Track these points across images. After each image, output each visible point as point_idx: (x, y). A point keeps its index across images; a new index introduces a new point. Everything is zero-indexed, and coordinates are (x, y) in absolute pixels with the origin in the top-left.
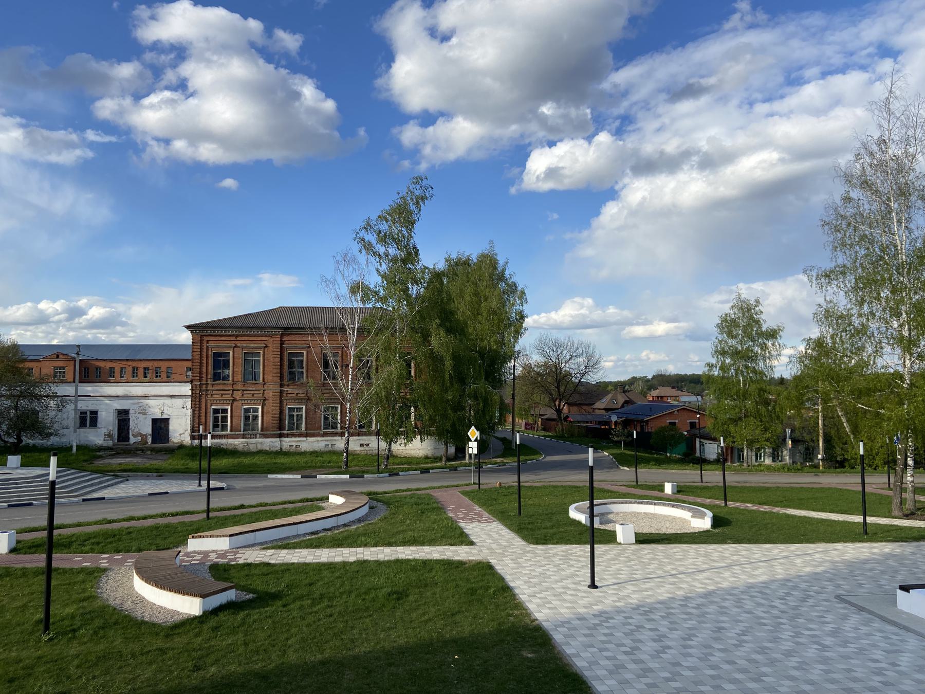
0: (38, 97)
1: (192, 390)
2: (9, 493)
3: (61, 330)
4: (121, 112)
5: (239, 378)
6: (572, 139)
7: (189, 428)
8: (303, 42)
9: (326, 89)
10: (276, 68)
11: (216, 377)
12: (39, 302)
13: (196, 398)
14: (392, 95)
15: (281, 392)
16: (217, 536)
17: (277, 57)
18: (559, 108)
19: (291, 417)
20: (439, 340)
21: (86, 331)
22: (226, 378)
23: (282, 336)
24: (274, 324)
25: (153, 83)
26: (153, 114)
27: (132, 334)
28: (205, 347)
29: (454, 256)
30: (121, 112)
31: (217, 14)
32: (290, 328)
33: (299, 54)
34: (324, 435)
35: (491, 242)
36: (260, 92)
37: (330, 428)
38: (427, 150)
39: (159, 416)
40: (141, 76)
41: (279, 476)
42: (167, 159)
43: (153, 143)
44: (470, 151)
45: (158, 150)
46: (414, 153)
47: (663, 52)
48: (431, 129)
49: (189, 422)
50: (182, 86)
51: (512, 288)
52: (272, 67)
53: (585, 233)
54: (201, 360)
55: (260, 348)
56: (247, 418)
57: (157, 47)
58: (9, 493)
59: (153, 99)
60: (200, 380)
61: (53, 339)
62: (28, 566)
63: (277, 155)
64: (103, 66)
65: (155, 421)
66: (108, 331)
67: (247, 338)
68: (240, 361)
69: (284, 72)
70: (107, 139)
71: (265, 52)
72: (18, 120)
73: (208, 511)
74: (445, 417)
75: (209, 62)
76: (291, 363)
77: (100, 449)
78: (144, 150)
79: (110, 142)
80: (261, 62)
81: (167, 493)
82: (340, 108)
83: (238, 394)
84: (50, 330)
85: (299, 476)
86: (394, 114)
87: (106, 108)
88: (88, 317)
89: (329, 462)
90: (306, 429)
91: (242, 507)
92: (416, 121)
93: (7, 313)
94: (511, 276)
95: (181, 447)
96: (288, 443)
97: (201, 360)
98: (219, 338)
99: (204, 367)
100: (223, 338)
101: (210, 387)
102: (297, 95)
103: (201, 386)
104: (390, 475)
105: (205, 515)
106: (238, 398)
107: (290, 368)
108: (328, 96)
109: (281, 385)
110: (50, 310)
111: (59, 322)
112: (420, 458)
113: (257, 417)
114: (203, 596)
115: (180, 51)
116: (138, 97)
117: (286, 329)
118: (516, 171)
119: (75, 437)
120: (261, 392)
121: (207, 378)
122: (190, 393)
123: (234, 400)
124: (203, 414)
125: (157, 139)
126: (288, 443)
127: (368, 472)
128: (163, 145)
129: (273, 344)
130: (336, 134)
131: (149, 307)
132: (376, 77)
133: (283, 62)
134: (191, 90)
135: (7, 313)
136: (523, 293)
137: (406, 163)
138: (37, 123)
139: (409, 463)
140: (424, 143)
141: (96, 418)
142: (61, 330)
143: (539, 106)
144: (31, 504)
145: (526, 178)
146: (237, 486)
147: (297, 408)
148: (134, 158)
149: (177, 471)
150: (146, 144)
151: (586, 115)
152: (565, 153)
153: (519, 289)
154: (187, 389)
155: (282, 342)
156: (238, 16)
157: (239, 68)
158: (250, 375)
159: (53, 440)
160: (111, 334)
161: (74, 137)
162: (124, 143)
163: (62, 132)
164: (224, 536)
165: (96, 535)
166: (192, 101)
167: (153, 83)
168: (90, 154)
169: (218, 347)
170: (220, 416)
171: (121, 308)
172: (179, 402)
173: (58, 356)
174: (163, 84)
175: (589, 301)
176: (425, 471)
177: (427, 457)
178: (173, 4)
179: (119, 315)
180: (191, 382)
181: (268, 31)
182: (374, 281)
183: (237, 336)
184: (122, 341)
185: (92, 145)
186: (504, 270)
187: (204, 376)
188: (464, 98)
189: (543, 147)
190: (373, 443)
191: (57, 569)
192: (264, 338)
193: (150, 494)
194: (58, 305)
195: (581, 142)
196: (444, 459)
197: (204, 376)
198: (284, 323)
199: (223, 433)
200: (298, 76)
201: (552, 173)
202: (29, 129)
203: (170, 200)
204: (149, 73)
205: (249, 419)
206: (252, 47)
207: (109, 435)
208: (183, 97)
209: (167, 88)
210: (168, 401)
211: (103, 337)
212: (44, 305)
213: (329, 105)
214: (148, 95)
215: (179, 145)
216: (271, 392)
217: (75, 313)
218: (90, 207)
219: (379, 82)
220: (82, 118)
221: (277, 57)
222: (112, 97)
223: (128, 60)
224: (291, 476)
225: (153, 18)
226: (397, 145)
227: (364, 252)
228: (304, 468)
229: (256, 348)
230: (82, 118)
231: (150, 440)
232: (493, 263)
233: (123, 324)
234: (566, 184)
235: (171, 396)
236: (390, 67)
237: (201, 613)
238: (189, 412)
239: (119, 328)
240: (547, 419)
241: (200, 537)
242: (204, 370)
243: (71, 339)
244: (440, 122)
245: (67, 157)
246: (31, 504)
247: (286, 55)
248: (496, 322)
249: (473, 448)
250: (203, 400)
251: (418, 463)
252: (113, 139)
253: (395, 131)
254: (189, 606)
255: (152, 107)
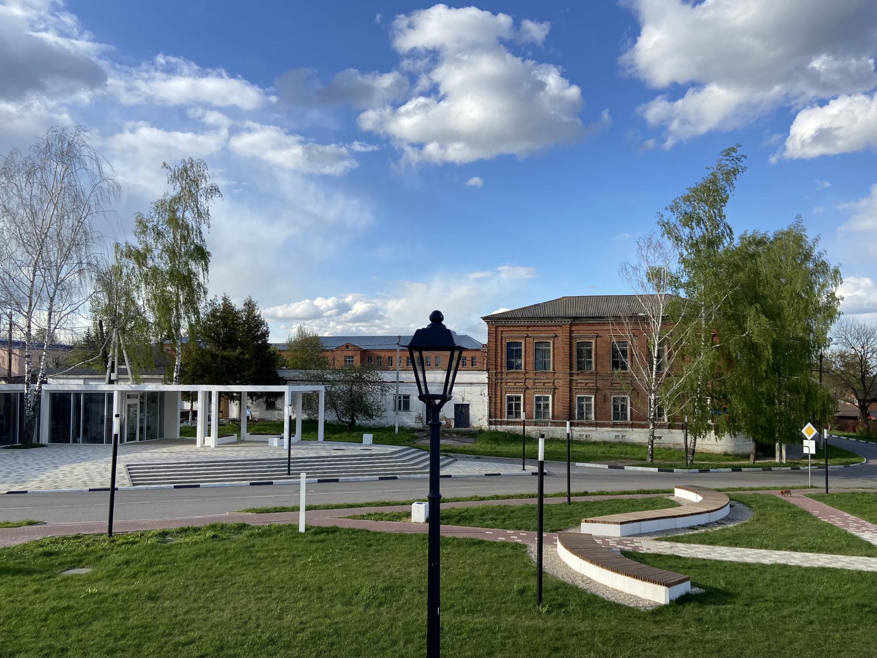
0: (314, 116)
1: (489, 378)
2: (376, 467)
3: (332, 324)
4: (382, 122)
5: (530, 367)
6: (850, 96)
7: (486, 413)
8: (550, 31)
9: (570, 76)
10: (523, 61)
11: (510, 366)
12: (314, 300)
13: (493, 386)
14: (637, 71)
15: (571, 381)
16: (609, 523)
17: (523, 49)
18: (836, 59)
19: (580, 407)
20: (756, 325)
21: (350, 324)
22: (519, 367)
23: (571, 325)
24: (562, 314)
25: (409, 90)
26: (408, 122)
27: (387, 327)
28: (499, 338)
29: (749, 233)
30: (382, 122)
31: (470, 14)
32: (579, 318)
33: (544, 43)
34: (614, 425)
35: (798, 216)
36: (508, 86)
37: (618, 417)
38: (675, 125)
39: (461, 402)
40: (398, 84)
41: (587, 465)
42: (420, 163)
43: (409, 149)
44: (724, 120)
45: (413, 155)
46: (661, 130)
47: (638, 12)
48: (680, 102)
49: (486, 408)
50: (434, 92)
51: (822, 267)
52: (519, 60)
53: (864, 202)
54: (496, 350)
55: (550, 338)
56: (538, 406)
57: (414, 54)
58: (376, 467)
59: (410, 106)
60: (496, 369)
61: (325, 331)
62: (457, 536)
63: (518, 148)
64: (367, 80)
65: (457, 406)
66: (369, 324)
67: (538, 328)
68: (531, 351)
69: (530, 63)
70: (370, 148)
71: (512, 46)
72: (298, 138)
73: (569, 495)
74: (759, 411)
75: (459, 62)
76: (579, 352)
77: (413, 430)
78: (401, 157)
79: (373, 151)
80: (509, 56)
81: (499, 475)
82: (584, 94)
83: (530, 383)
84: (322, 323)
85: (607, 466)
86: (641, 91)
87: (369, 119)
88: (353, 312)
89: (626, 453)
90: (596, 419)
91: (586, 494)
92: (664, 96)
93: (290, 309)
94: (820, 254)
95: (481, 431)
96: (579, 432)
97: (496, 350)
98: (511, 328)
99: (499, 356)
100: (516, 329)
101: (504, 376)
102: (542, 85)
103: (496, 374)
104: (701, 471)
105: (566, 499)
106: (530, 386)
107: (579, 357)
108: (571, 83)
109: (571, 375)
110: (323, 307)
111: (331, 316)
112: (719, 455)
113: (548, 405)
114: (668, 585)
115: (433, 56)
116: (396, 105)
117: (575, 318)
118: (777, 137)
119: (393, 418)
120: (551, 381)
121: (501, 366)
122: (487, 381)
123: (527, 388)
124: (499, 401)
125: (412, 145)
126: (579, 432)
127: (676, 467)
128: (417, 149)
129: (563, 334)
130: (579, 121)
131: (402, 301)
132: (620, 54)
133: (530, 54)
134: (442, 93)
135: (290, 309)
136: (836, 272)
137: (651, 143)
138: (314, 139)
139: (710, 459)
140: (671, 119)
141: (408, 402)
142: (332, 324)
143: (811, 61)
144: (396, 478)
145: (789, 143)
146: (555, 472)
147: (586, 398)
148: (393, 165)
149: (491, 454)
150: (402, 151)
151: (868, 66)
152: (840, 112)
153: (832, 268)
154: (483, 377)
155: (571, 332)
156: (489, 13)
157: (488, 65)
158: (541, 365)
159: (375, 422)
160: (372, 326)
161: (344, 150)
162: (385, 148)
163: (333, 146)
164: (615, 523)
165: (493, 510)
166: (444, 105)
167: (409, 90)
168: (356, 164)
169: (511, 337)
170: (514, 403)
171: (379, 303)
172: (477, 389)
173: (347, 347)
174: (418, 89)
175: (867, 281)
176: (737, 469)
177: (726, 454)
178: (429, 10)
179: (377, 310)
180: (488, 370)
181: (517, 25)
182: (675, 267)
183: (529, 327)
184: (379, 333)
185: (357, 156)
186: (811, 249)
187: (499, 364)
188: (721, 62)
189: (812, 107)
190: (676, 438)
191: (447, 542)
192: (554, 328)
193: (486, 475)
194: (330, 302)
195: (863, 98)
196: (752, 457)
197: (499, 364)
198: (572, 312)
199: (517, 420)
200: (544, 65)
201: (822, 136)
202: (307, 146)
203: (419, 199)
204: (406, 80)
205: (540, 408)
206: (500, 43)
207: (419, 418)
208: (435, 102)
209: (422, 94)
210: (468, 388)
211: (364, 330)
212: (319, 302)
213: (574, 92)
214: (404, 103)
215: (432, 148)
216: (561, 382)
217: (344, 308)
218: (353, 212)
219: (624, 59)
220: (350, 132)
221: (523, 49)
222: (374, 109)
223: (388, 71)
224: (598, 466)
225: (411, 26)
226: (642, 123)
227: (666, 235)
228: (611, 458)
229: (544, 338)
230: (350, 132)
231: (453, 424)
232: (799, 240)
233: (381, 318)
234: (841, 146)
235: (471, 384)
236: (635, 42)
237: (668, 602)
238: (486, 399)
239: (377, 321)
240: (840, 417)
241: (592, 522)
242: (499, 360)
243: (339, 331)
244: (689, 95)
245: (337, 169)
246: (396, 478)
247: (532, 45)
248: (802, 306)
249: (809, 447)
250: (499, 388)
251: (719, 460)
252: (375, 148)
253: (639, 109)
254: (654, 594)
255: (408, 114)
